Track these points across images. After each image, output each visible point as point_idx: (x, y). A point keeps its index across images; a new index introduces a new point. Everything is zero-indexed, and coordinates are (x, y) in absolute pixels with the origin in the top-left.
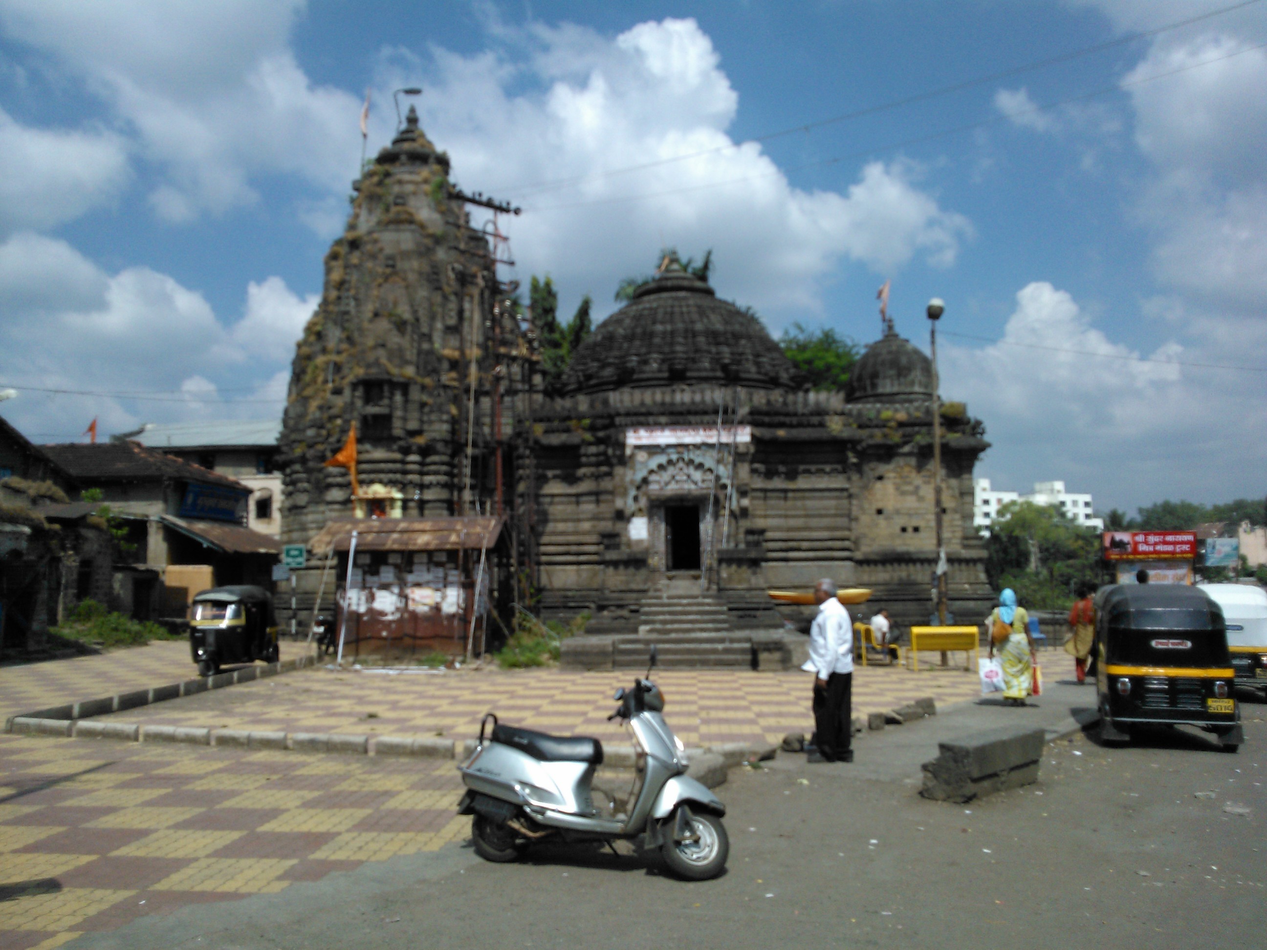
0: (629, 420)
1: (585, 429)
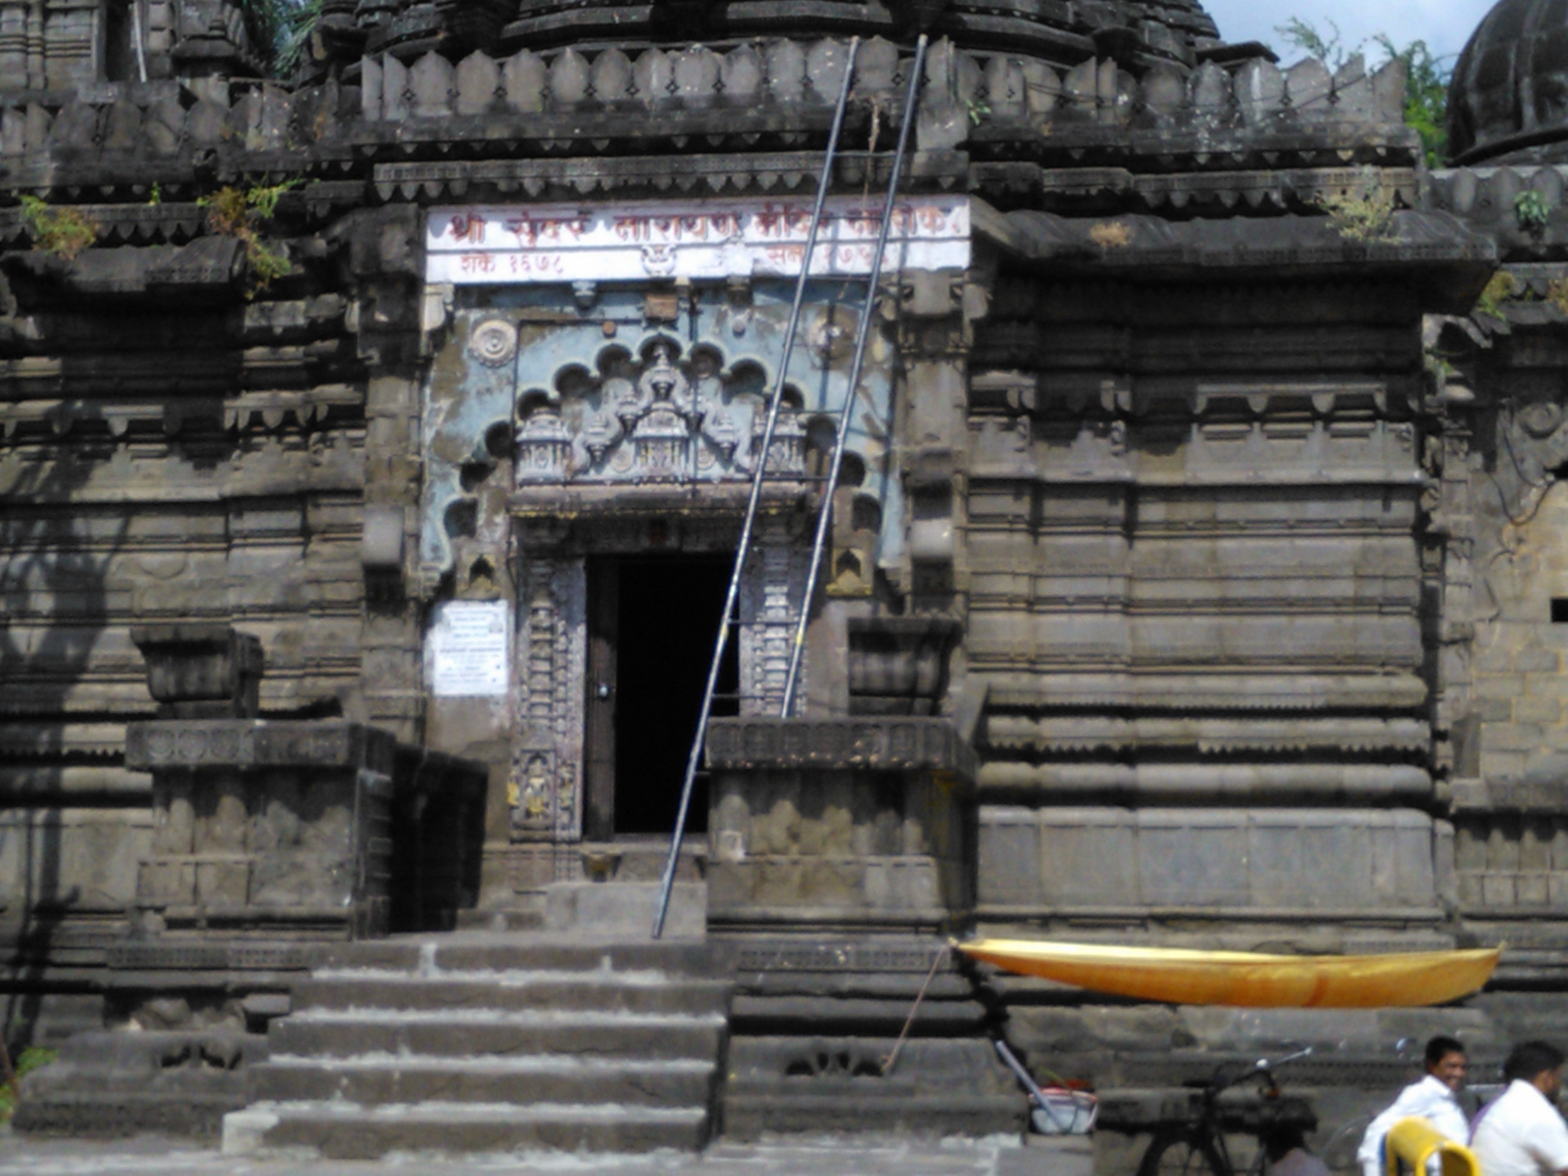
0: (432, 175)
1: (266, 230)
